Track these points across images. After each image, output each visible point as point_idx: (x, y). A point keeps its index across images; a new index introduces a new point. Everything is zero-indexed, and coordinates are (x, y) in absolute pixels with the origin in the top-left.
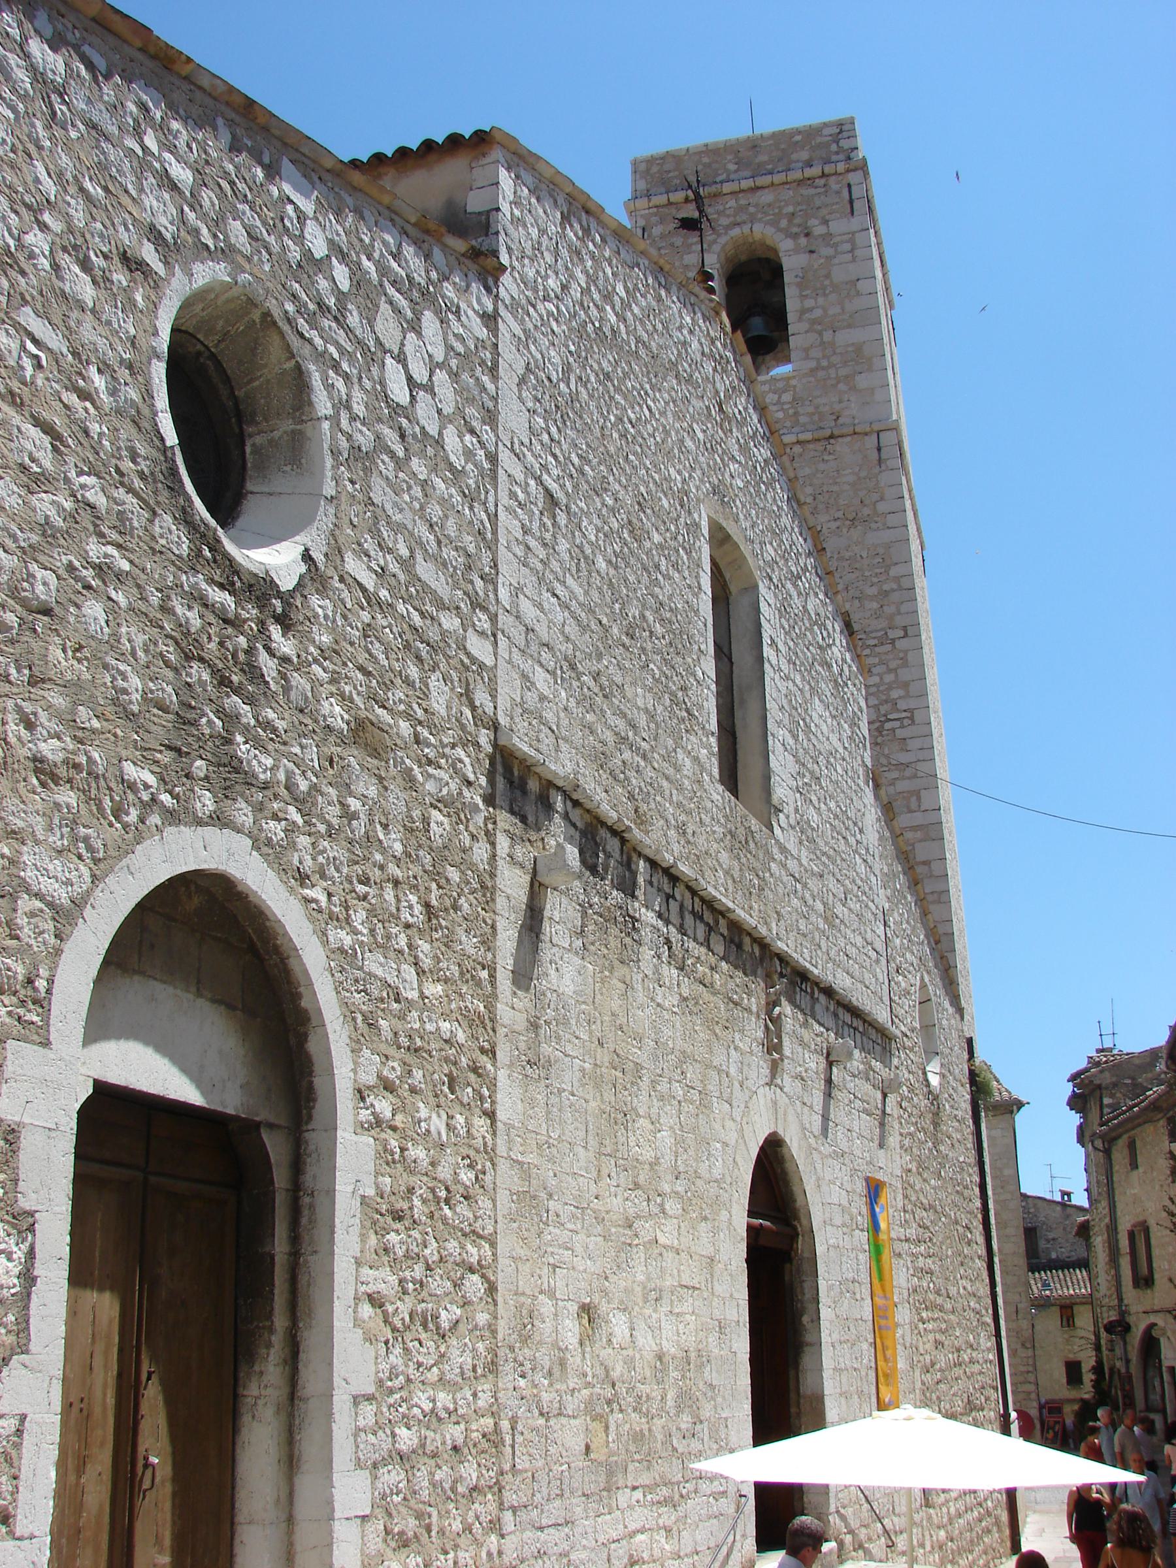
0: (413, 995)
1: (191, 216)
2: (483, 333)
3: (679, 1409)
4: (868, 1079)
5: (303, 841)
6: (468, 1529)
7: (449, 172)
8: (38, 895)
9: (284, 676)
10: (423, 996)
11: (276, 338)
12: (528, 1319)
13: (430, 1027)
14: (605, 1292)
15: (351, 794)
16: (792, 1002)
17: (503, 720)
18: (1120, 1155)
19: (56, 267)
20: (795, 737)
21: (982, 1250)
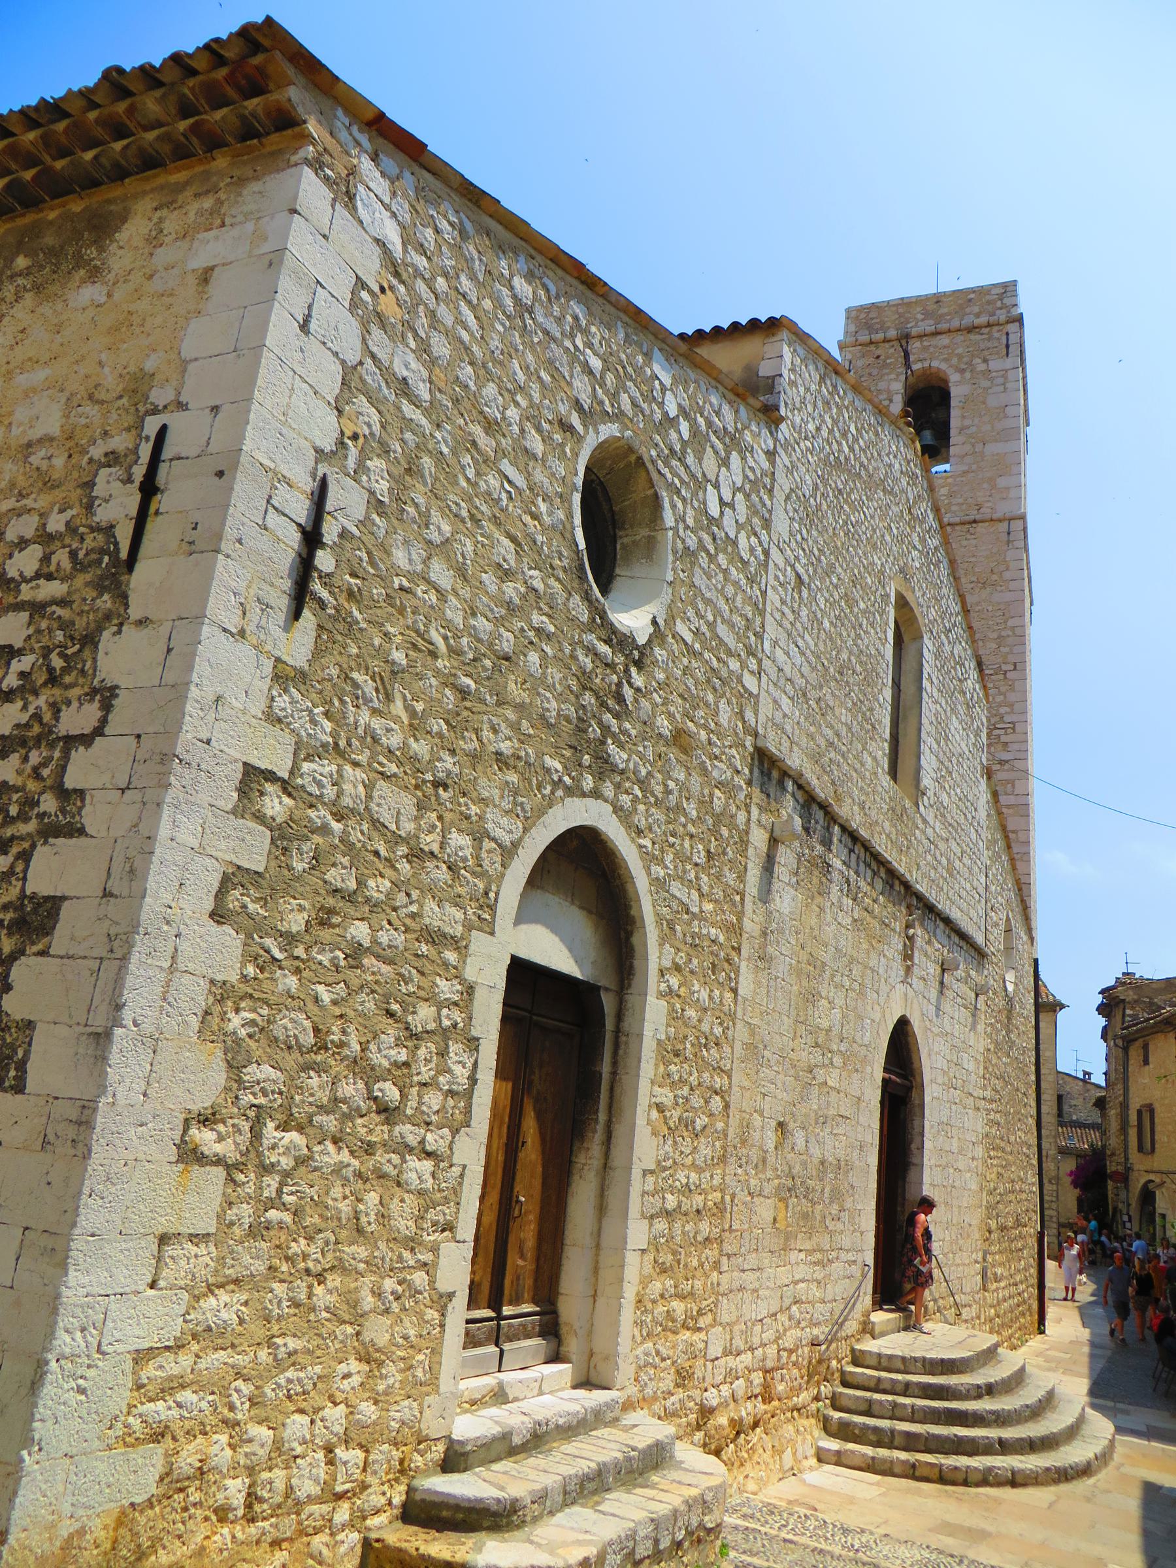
0: (696, 910)
1: (599, 391)
2: (766, 465)
3: (832, 1201)
5: (641, 807)
6: (701, 1265)
7: (747, 348)
8: (494, 839)
9: (636, 700)
10: (702, 911)
11: (643, 474)
12: (746, 1127)
13: (704, 931)
15: (670, 778)
16: (922, 925)
17: (761, 731)
18: (1135, 1053)
19: (522, 431)
20: (938, 744)
21: (1034, 1112)
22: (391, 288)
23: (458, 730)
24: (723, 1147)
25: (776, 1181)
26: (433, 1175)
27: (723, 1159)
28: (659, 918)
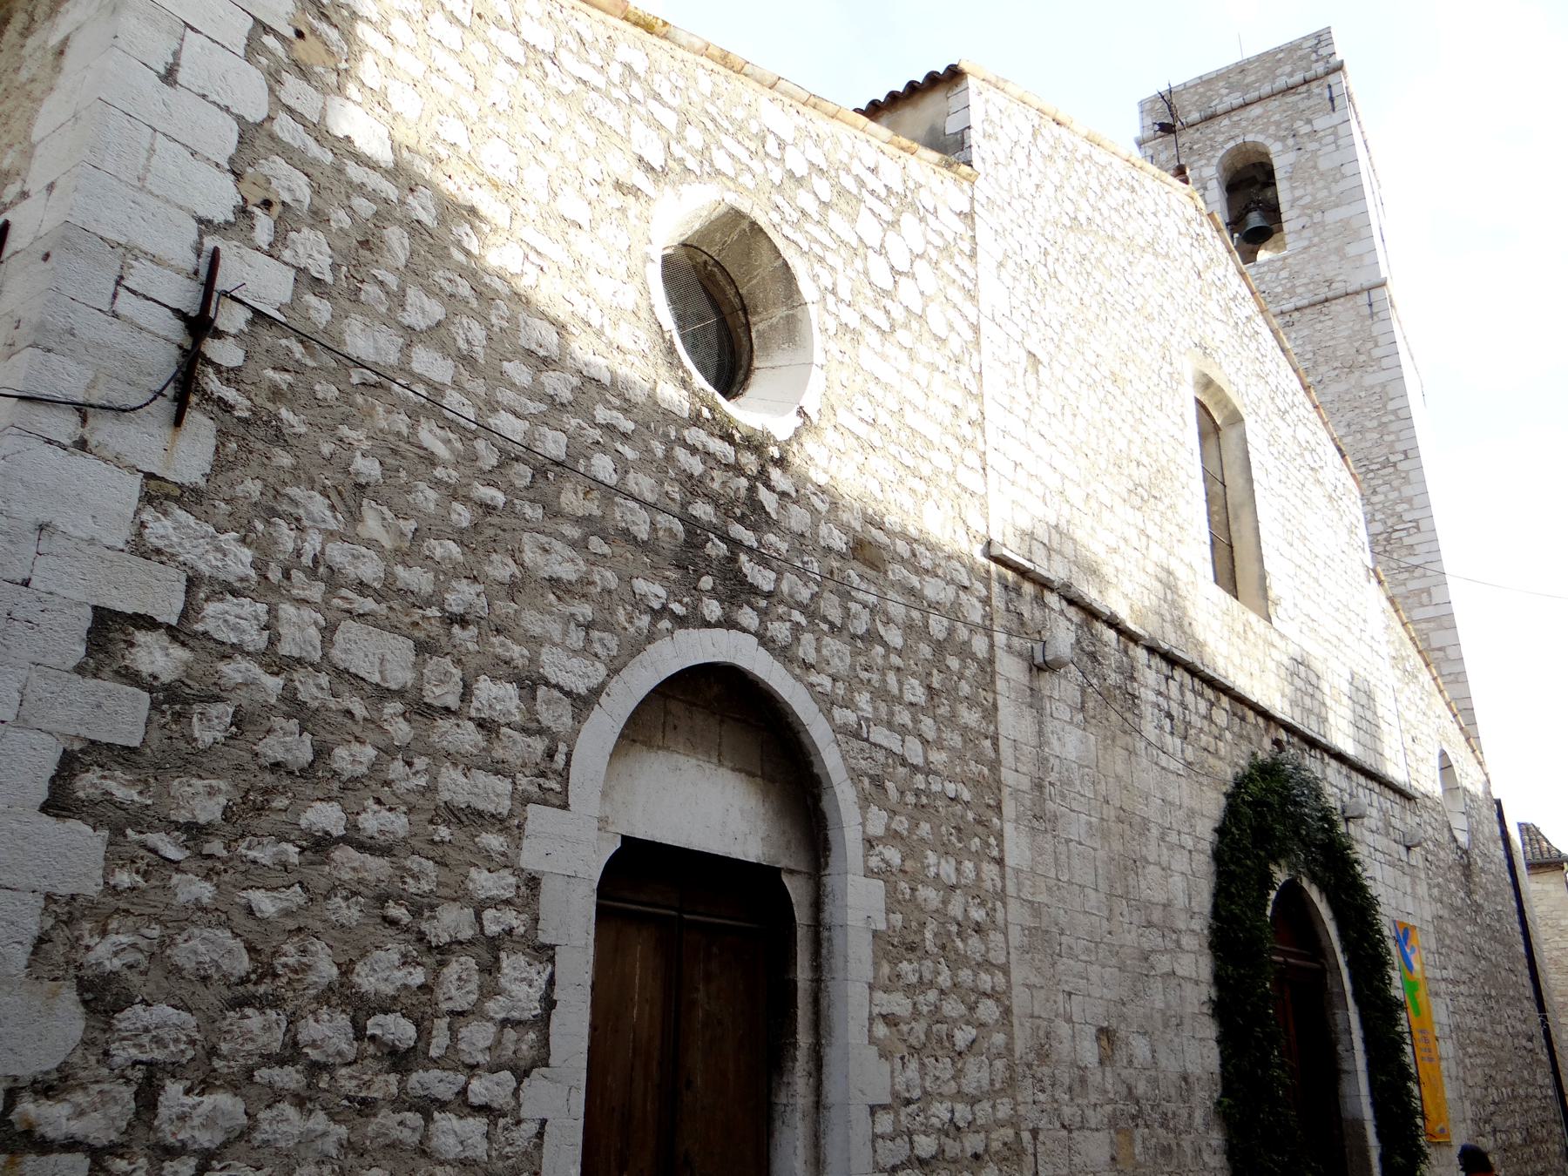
4: (1388, 834)
14: (1123, 1018)
22: (313, 31)
23: (480, 552)
24: (1009, 1067)
25: (1109, 1108)
26: (487, 1136)
27: (1011, 1082)
28: (855, 775)
